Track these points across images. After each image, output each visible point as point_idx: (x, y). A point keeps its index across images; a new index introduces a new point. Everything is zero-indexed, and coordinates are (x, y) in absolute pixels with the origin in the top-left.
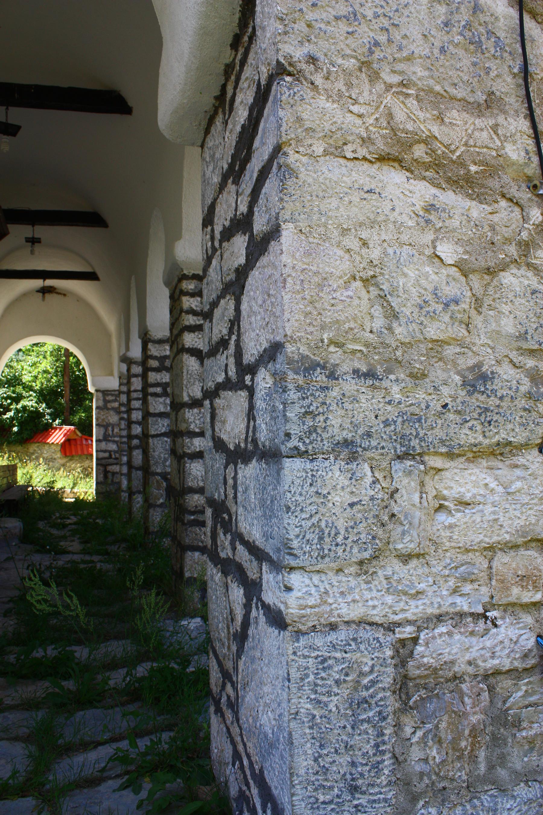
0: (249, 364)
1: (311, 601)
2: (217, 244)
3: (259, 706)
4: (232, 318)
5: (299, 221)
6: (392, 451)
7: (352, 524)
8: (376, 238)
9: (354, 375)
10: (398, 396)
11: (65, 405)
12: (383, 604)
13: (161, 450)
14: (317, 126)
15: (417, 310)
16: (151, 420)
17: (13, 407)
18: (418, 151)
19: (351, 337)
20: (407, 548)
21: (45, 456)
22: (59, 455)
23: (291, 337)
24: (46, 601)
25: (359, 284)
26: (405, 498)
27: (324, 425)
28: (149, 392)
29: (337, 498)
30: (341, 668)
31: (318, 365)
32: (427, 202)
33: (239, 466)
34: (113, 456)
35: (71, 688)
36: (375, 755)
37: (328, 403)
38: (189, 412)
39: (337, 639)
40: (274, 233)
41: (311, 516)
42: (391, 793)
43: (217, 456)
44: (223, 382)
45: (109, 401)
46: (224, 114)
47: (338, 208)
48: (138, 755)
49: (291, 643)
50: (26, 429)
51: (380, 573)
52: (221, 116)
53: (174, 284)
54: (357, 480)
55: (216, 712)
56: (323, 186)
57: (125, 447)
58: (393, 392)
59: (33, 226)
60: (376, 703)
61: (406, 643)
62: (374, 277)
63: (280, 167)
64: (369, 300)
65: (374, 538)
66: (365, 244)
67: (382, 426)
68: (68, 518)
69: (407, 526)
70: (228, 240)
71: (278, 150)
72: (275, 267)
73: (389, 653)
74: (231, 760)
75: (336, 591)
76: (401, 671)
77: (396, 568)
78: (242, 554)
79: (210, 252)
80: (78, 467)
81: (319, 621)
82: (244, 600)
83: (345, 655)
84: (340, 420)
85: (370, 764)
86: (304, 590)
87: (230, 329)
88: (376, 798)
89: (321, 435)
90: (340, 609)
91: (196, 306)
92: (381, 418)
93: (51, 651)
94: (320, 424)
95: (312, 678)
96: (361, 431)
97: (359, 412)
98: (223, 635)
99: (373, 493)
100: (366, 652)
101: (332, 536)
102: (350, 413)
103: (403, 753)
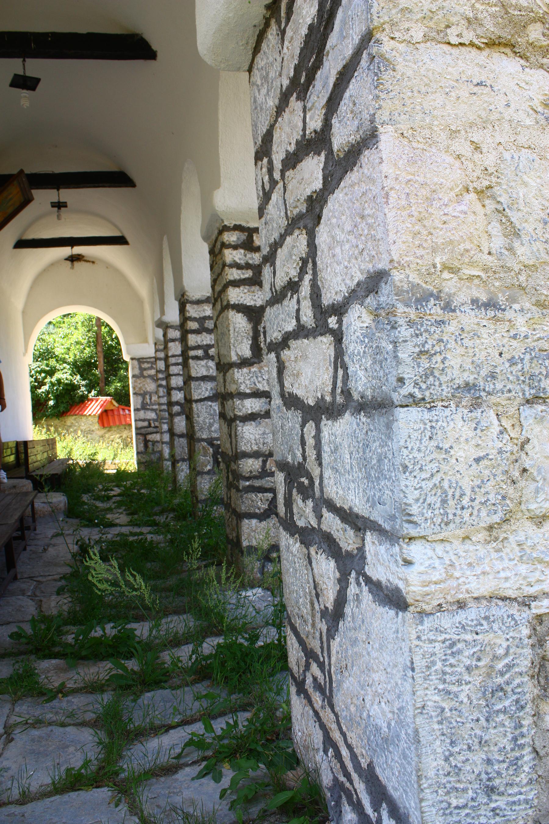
0: (333, 304)
1: (436, 576)
2: (277, 175)
3: (367, 694)
4: (304, 256)
5: (400, 123)
6: (520, 394)
7: (479, 482)
8: (490, 140)
9: (473, 305)
10: (524, 329)
11: (99, 376)
12: (516, 575)
13: (206, 415)
14: (415, 6)
15: (541, 226)
16: (193, 384)
17: (48, 380)
18: (533, 32)
19: (467, 260)
20: (541, 508)
21: (83, 428)
22: (97, 426)
23: (399, 263)
24: (107, 580)
25: (473, 196)
26: (537, 449)
27: (442, 366)
28: (190, 355)
29: (461, 453)
30: (472, 652)
31: (432, 295)
32: (546, 95)
33: (324, 422)
34: (153, 425)
35: (136, 668)
36: (513, 750)
37: (445, 340)
38: (238, 372)
39: (466, 619)
40: (369, 139)
41: (432, 475)
42: (533, 793)
43: (289, 414)
44: (294, 330)
45: (145, 369)
46: (279, 23)
47: (444, 106)
48: (214, 739)
49: (414, 626)
50: (62, 402)
51: (512, 538)
52: (274, 28)
53: (214, 237)
54: (482, 431)
55: (298, 693)
56: (425, 80)
57: (166, 415)
58: (518, 324)
59: (58, 190)
60: (513, 690)
61: (544, 619)
62: (490, 187)
63: (372, 58)
64: (485, 215)
65: (504, 498)
66: (477, 148)
67: (507, 365)
68: (112, 490)
69: (541, 482)
70: (294, 167)
71: (368, 38)
72: (372, 180)
73: (526, 631)
74: (321, 746)
75: (463, 562)
76: (539, 651)
77: (530, 532)
78: (332, 523)
79: (267, 187)
80: (116, 437)
81: (445, 598)
82: (338, 575)
83: (476, 637)
84: (459, 360)
85: (508, 760)
86: (427, 563)
87: (301, 269)
88: (515, 799)
89: (438, 379)
90: (469, 583)
91: (240, 259)
92: (506, 356)
93: (110, 630)
94: (437, 366)
95: (439, 665)
96: (484, 373)
97: (480, 350)
98: (306, 611)
99: (501, 445)
100: (500, 632)
101: (457, 497)
102: (471, 351)
103: (544, 747)
